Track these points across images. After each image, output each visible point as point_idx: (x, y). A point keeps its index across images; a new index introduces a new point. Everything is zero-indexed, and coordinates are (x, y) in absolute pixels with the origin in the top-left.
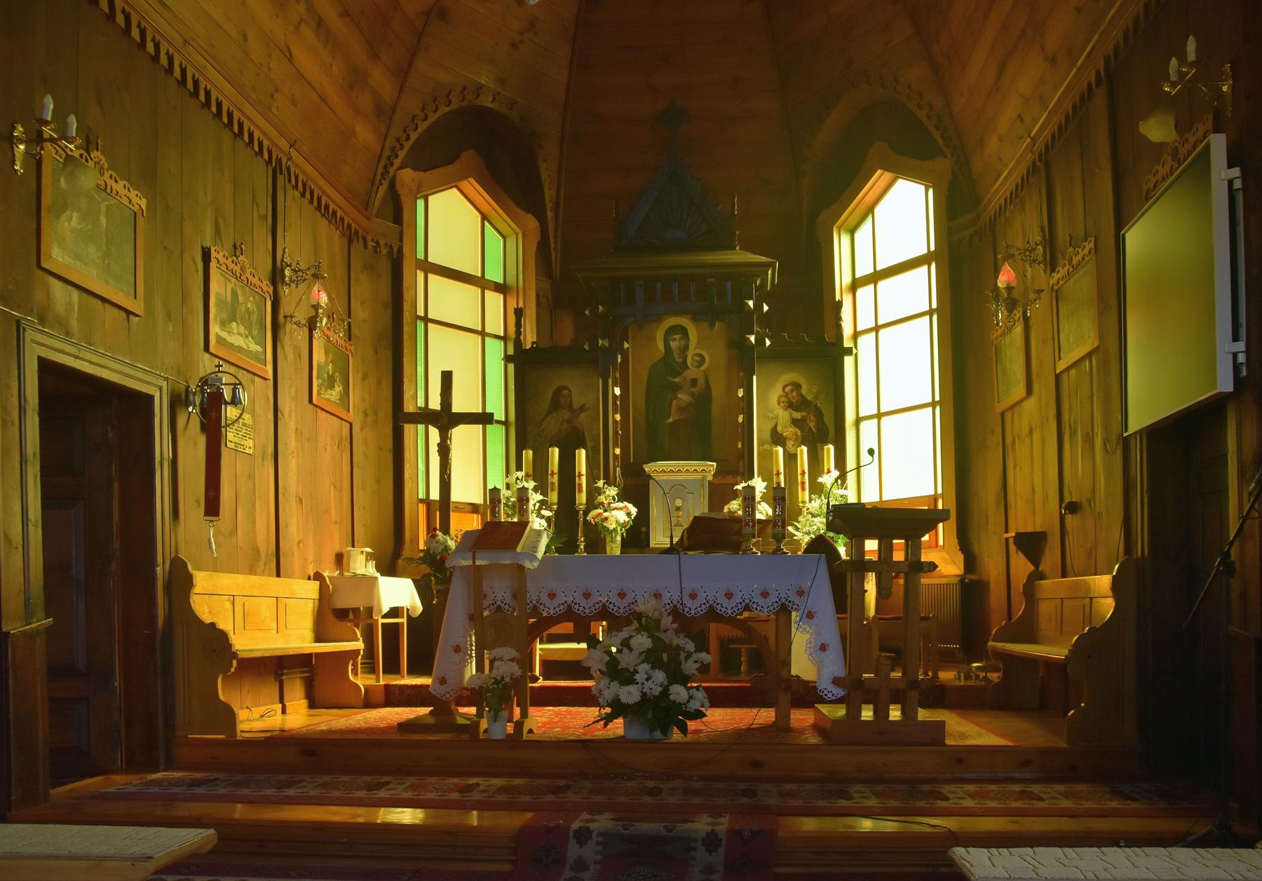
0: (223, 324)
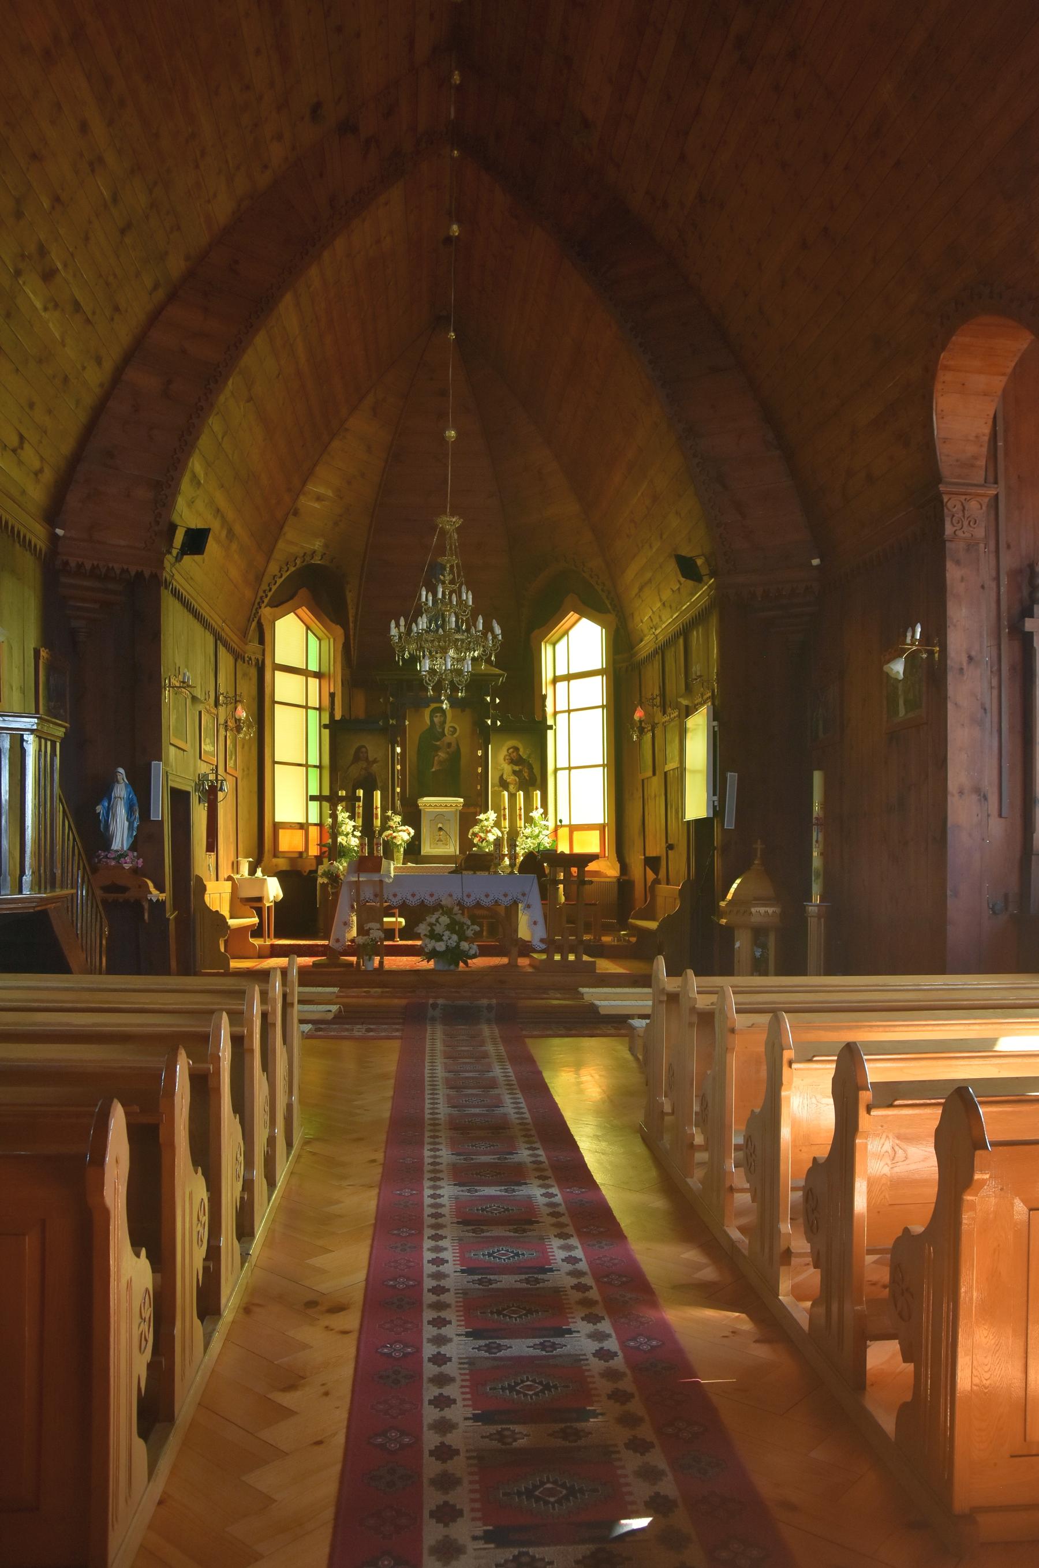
0: (205, 745)
